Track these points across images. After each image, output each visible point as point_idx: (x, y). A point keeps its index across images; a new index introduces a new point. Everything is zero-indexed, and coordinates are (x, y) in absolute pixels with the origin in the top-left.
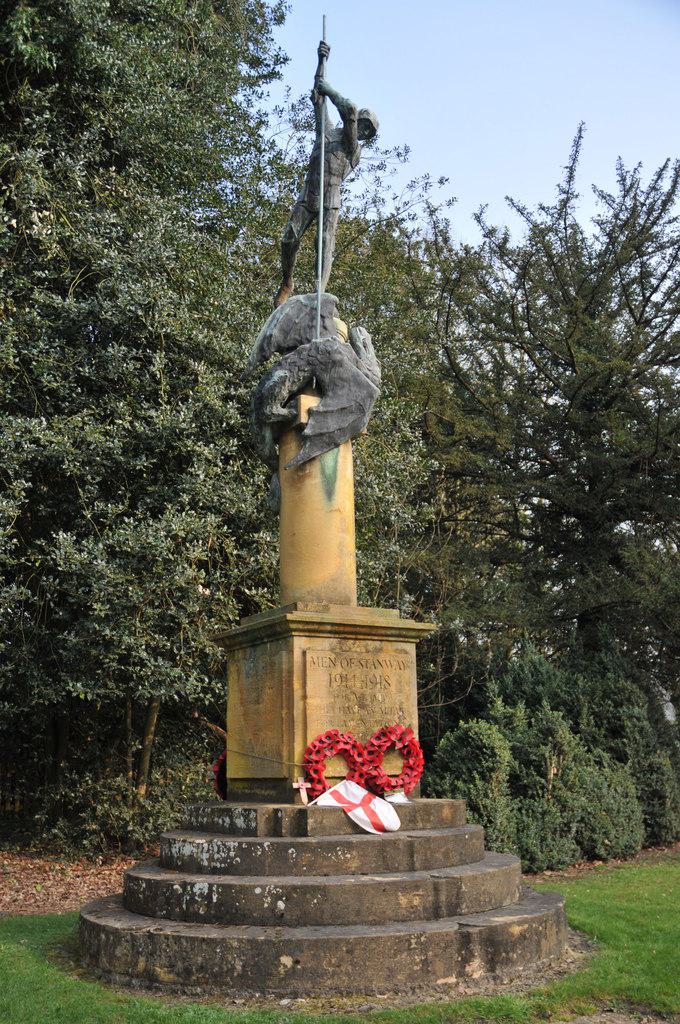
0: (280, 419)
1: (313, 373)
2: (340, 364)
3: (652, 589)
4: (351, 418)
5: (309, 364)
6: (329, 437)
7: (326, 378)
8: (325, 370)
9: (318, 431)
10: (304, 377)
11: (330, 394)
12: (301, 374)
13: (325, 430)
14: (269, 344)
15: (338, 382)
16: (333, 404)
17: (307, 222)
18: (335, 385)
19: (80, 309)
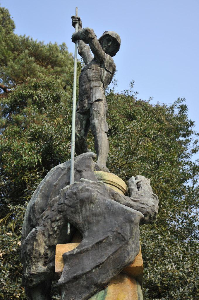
0: (43, 278)
1: (66, 220)
2: (90, 200)
3: (164, 141)
4: (110, 250)
5: (60, 212)
6: (87, 278)
7: (79, 219)
8: (76, 212)
9: (71, 276)
10: (58, 227)
11: (86, 234)
12: (54, 225)
13: (80, 272)
14: (34, 212)
15: (94, 219)
16: (88, 242)
17: (84, 122)
18: (89, 223)
19: (196, 294)
